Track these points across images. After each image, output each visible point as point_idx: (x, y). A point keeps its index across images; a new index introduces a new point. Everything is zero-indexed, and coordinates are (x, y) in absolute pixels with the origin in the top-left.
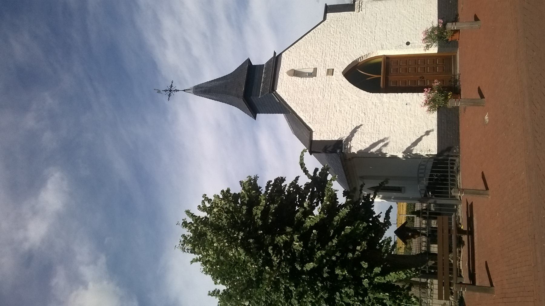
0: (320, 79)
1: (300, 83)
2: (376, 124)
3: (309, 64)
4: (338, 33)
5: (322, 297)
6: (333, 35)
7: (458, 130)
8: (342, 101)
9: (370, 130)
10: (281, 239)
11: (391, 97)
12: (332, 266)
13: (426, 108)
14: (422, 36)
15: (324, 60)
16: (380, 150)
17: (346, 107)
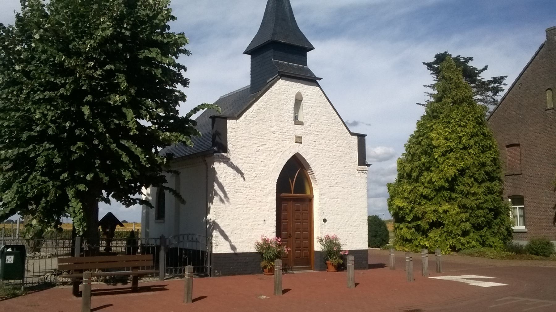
0: (292, 129)
1: (289, 106)
2: (245, 189)
3: (308, 116)
4: (338, 148)
5: (49, 127)
6: (336, 143)
7: (238, 274)
8: (268, 153)
9: (238, 182)
10: (122, 81)
11: (272, 205)
12: (88, 140)
13: (261, 241)
14: (331, 235)
15: (311, 133)
16: (216, 194)
17: (262, 157)
